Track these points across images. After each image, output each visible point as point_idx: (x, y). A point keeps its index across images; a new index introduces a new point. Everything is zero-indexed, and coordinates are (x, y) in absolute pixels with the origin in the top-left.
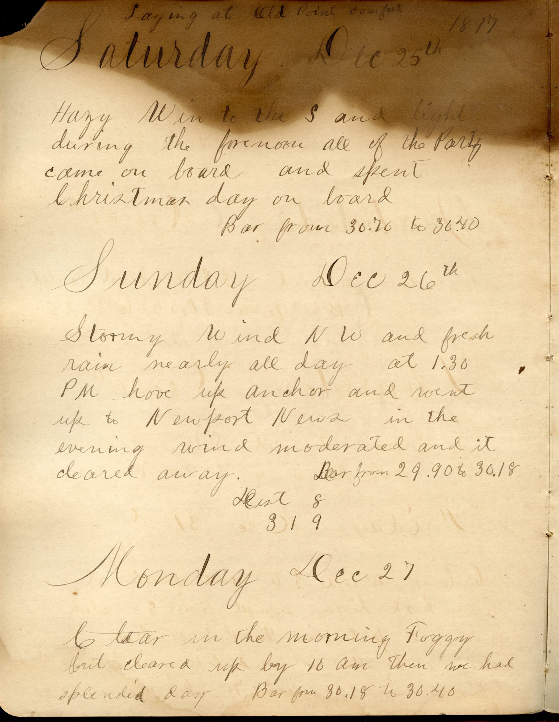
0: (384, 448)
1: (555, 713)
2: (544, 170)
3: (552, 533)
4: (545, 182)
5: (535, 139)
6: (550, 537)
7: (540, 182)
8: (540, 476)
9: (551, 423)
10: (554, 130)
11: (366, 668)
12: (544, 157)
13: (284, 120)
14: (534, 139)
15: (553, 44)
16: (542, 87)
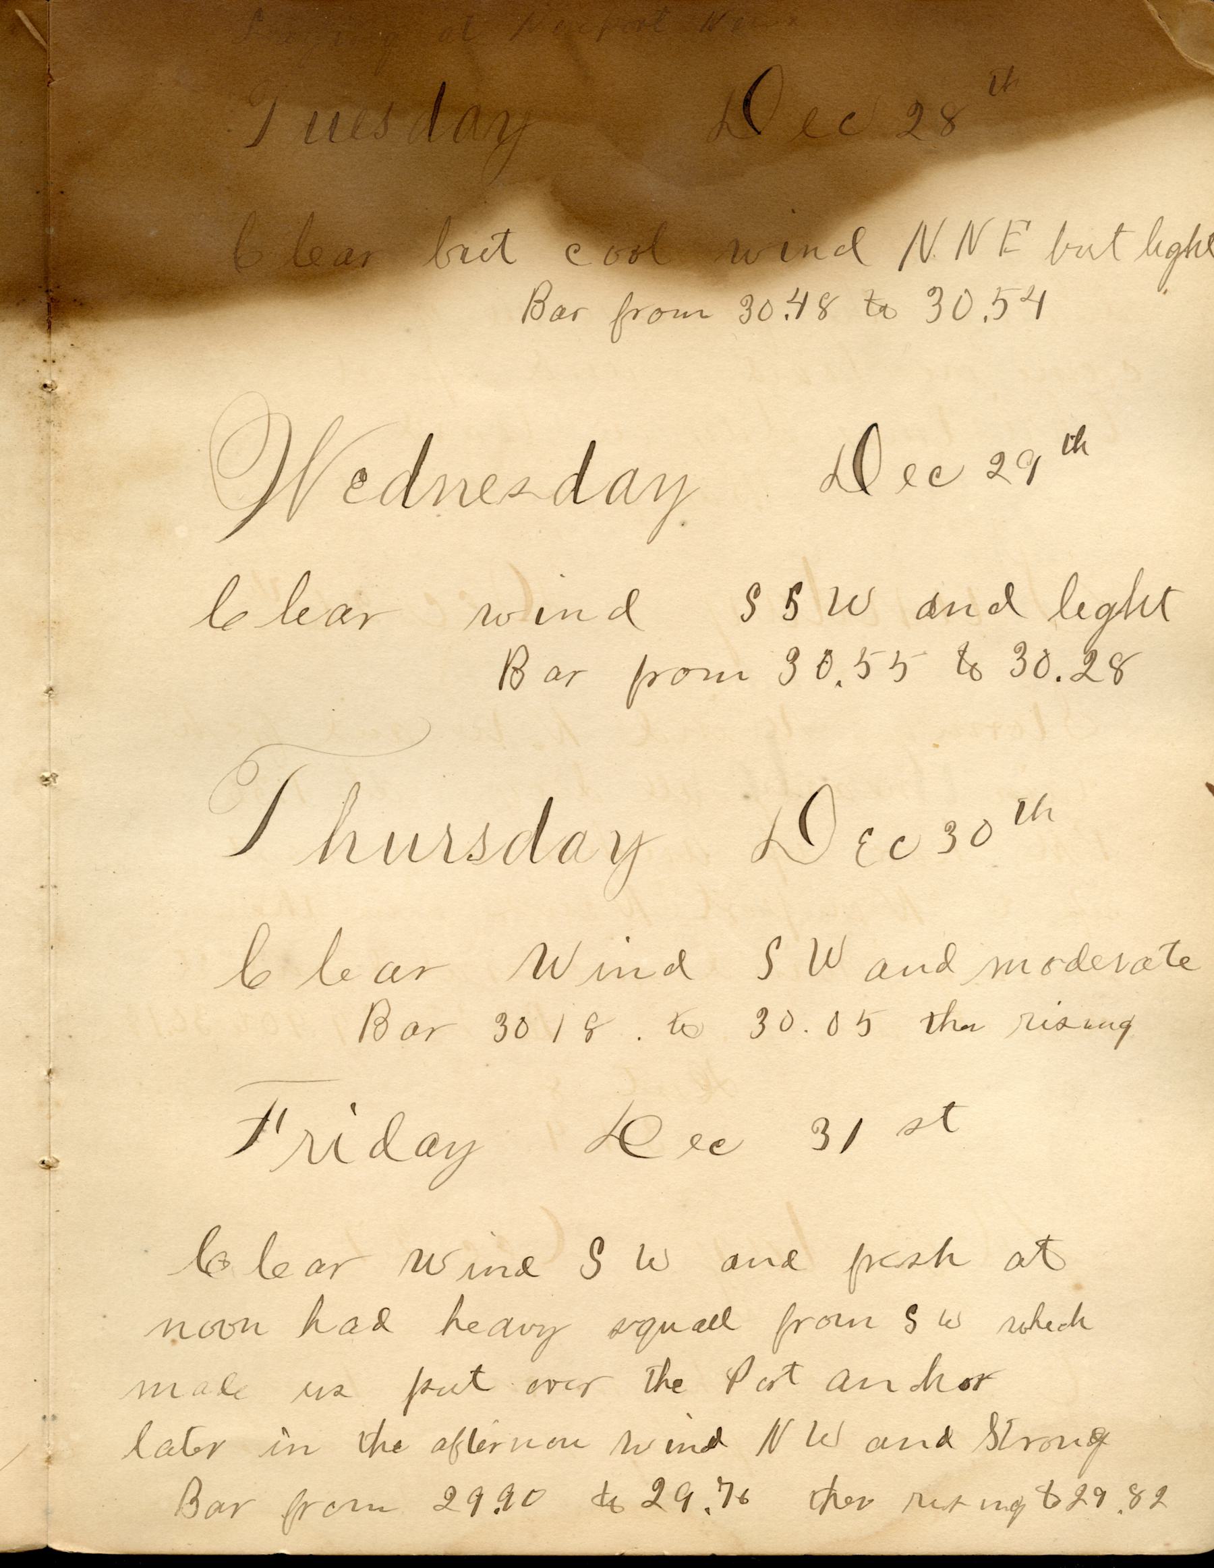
0: (473, 1328)
1: (75, 1551)
2: (38, 371)
3: (58, 1161)
4: (41, 397)
5: (21, 306)
6: (51, 1169)
7: (30, 398)
8: (27, 1037)
9: (52, 921)
10: (56, 285)
11: (277, 1451)
12: (38, 342)
13: (660, 262)
14: (18, 304)
15: (53, 99)
16: (37, 193)
